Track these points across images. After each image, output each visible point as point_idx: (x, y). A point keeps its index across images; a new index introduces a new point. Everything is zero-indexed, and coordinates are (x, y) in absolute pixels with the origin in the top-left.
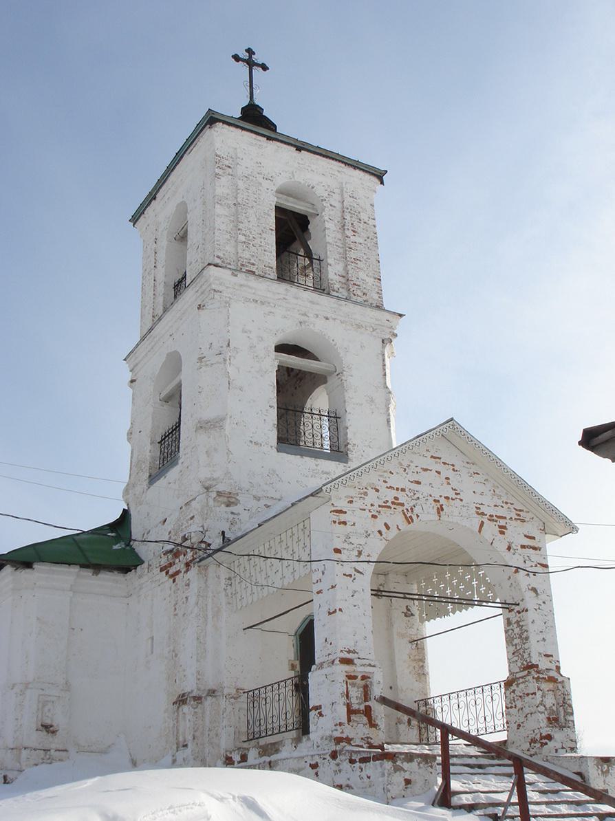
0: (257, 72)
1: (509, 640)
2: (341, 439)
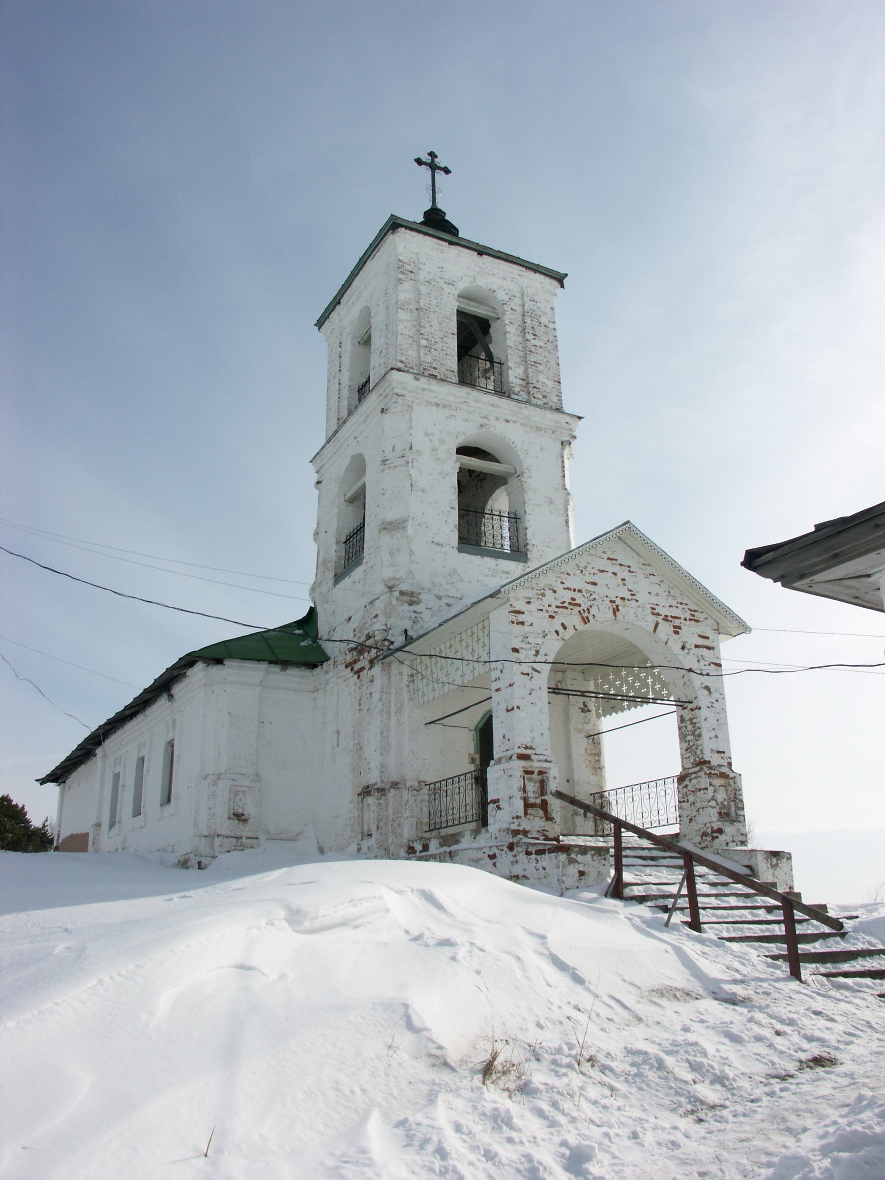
0: (439, 175)
1: (683, 737)
2: (521, 540)
